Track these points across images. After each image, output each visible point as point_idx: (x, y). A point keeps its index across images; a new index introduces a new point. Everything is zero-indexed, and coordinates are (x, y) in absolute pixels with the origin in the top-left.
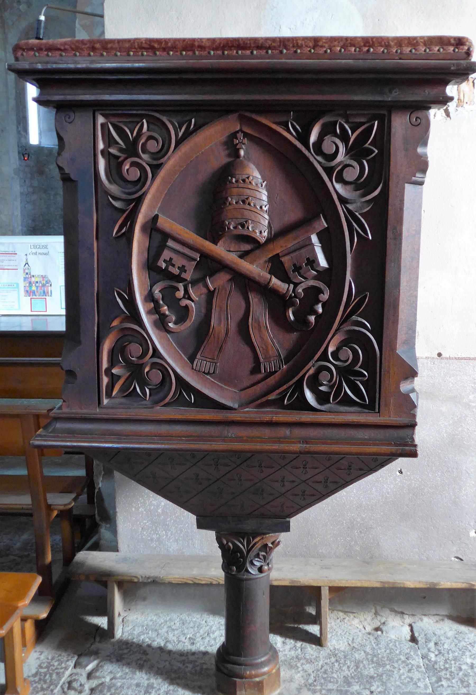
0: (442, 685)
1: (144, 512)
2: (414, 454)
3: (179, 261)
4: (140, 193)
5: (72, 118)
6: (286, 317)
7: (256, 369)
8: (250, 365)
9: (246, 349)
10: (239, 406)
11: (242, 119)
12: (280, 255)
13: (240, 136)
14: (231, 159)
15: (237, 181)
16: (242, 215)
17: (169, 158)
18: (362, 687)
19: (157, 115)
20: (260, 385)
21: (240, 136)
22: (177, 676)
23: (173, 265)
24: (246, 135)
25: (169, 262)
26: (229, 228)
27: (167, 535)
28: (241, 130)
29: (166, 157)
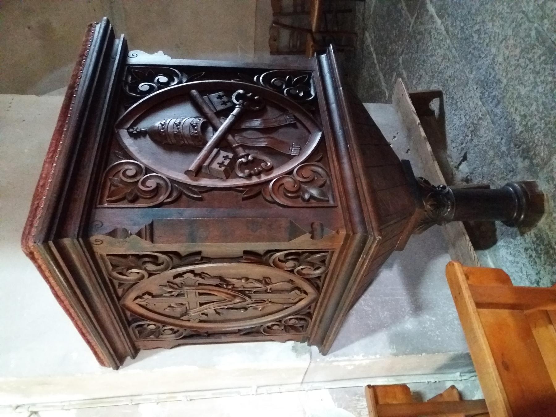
0: (481, 115)
1: (439, 331)
2: (373, 388)
3: (220, 159)
4: (167, 180)
5: (99, 223)
6: (257, 111)
7: (294, 126)
8: (292, 130)
9: (281, 130)
10: (320, 130)
11: (121, 125)
12: (215, 111)
13: (131, 130)
14: (148, 136)
15: (163, 129)
16: (187, 126)
17: (142, 163)
18: (501, 146)
19: (108, 169)
20: (305, 123)
21: (131, 130)
22: (550, 249)
23: (223, 162)
24: (131, 127)
25: (221, 164)
26: (196, 133)
27: (452, 314)
28: (128, 129)
29: (141, 165)
